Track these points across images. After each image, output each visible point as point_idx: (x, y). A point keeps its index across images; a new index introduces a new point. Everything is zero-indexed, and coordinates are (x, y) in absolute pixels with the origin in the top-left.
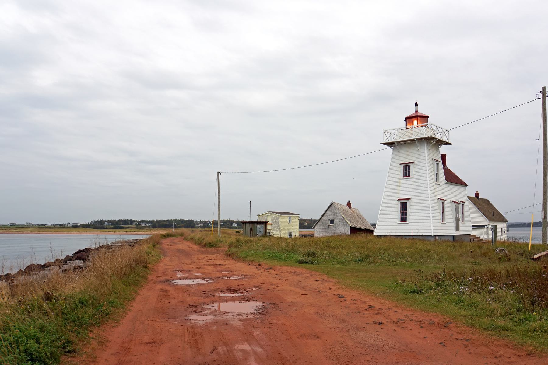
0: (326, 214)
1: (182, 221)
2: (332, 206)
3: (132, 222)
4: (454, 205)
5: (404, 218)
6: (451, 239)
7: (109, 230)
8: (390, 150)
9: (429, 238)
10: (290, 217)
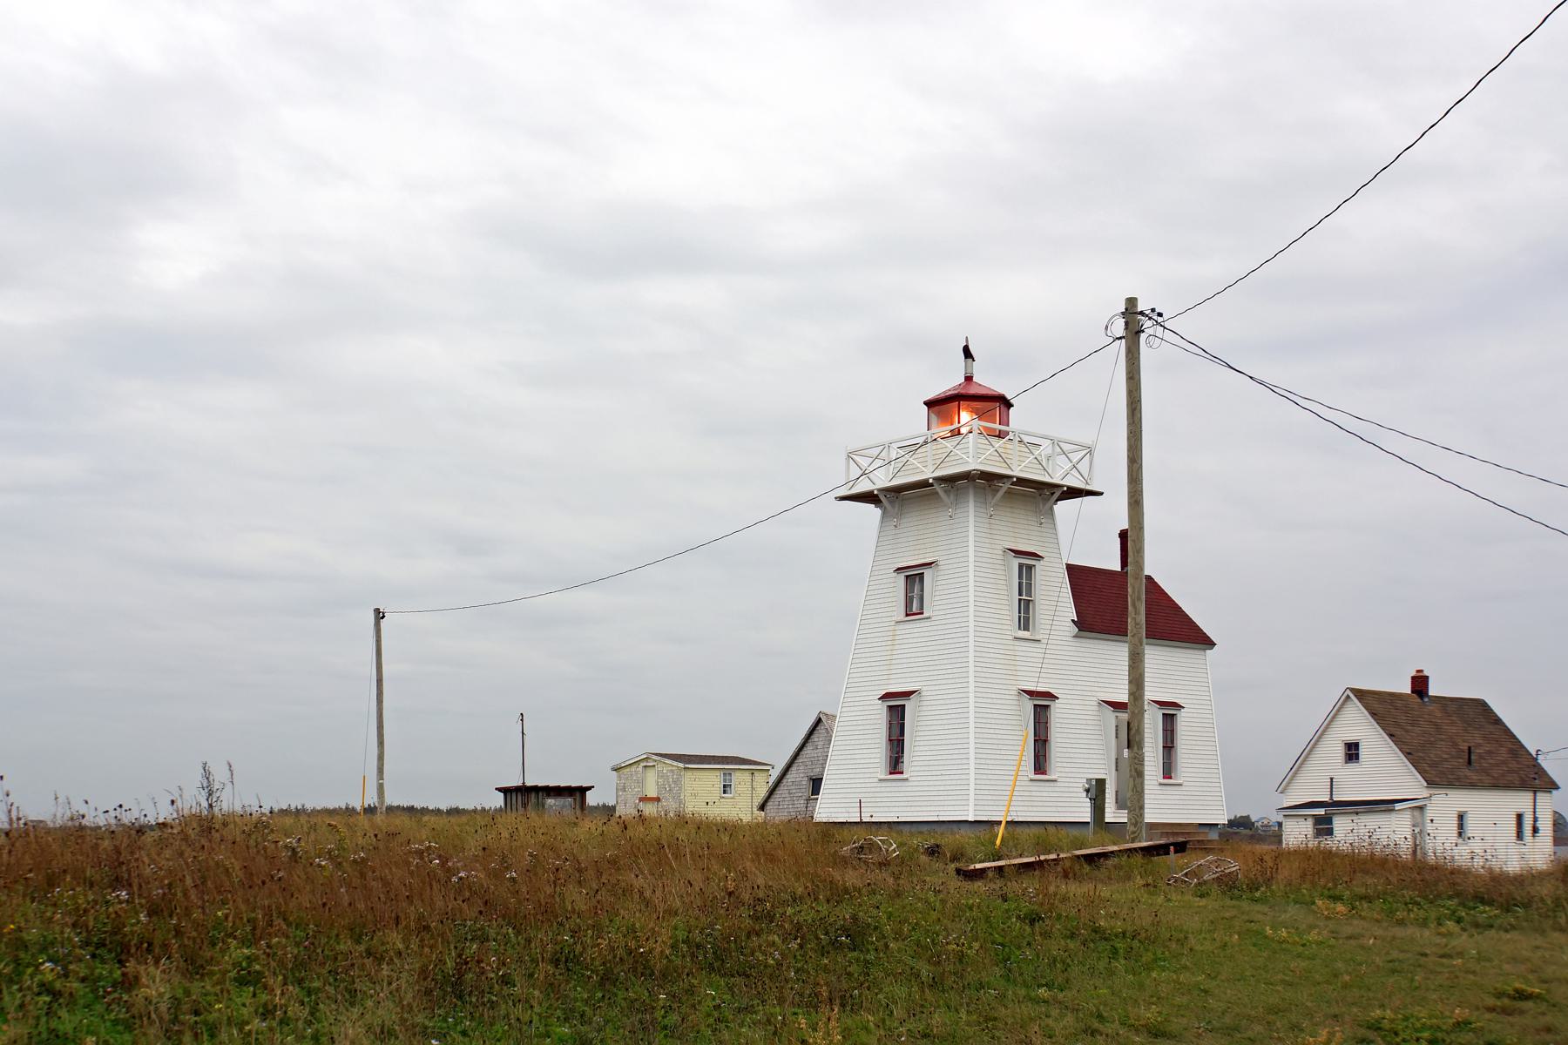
0: (800, 760)
4: (1111, 716)
8: (871, 512)
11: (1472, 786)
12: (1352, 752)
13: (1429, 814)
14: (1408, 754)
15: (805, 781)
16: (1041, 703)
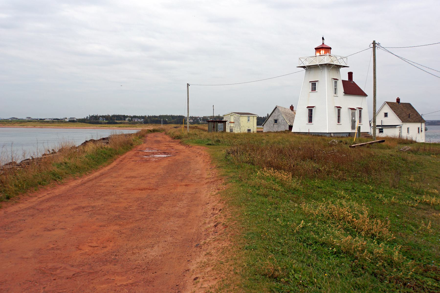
1: (173, 117)
2: (277, 109)
3: (125, 117)
4: (350, 111)
5: (310, 121)
6: (348, 135)
7: (104, 125)
9: (326, 134)
10: (249, 117)
11: (410, 122)
12: (386, 115)
13: (402, 128)
14: (398, 116)
15: (273, 120)
16: (339, 108)
